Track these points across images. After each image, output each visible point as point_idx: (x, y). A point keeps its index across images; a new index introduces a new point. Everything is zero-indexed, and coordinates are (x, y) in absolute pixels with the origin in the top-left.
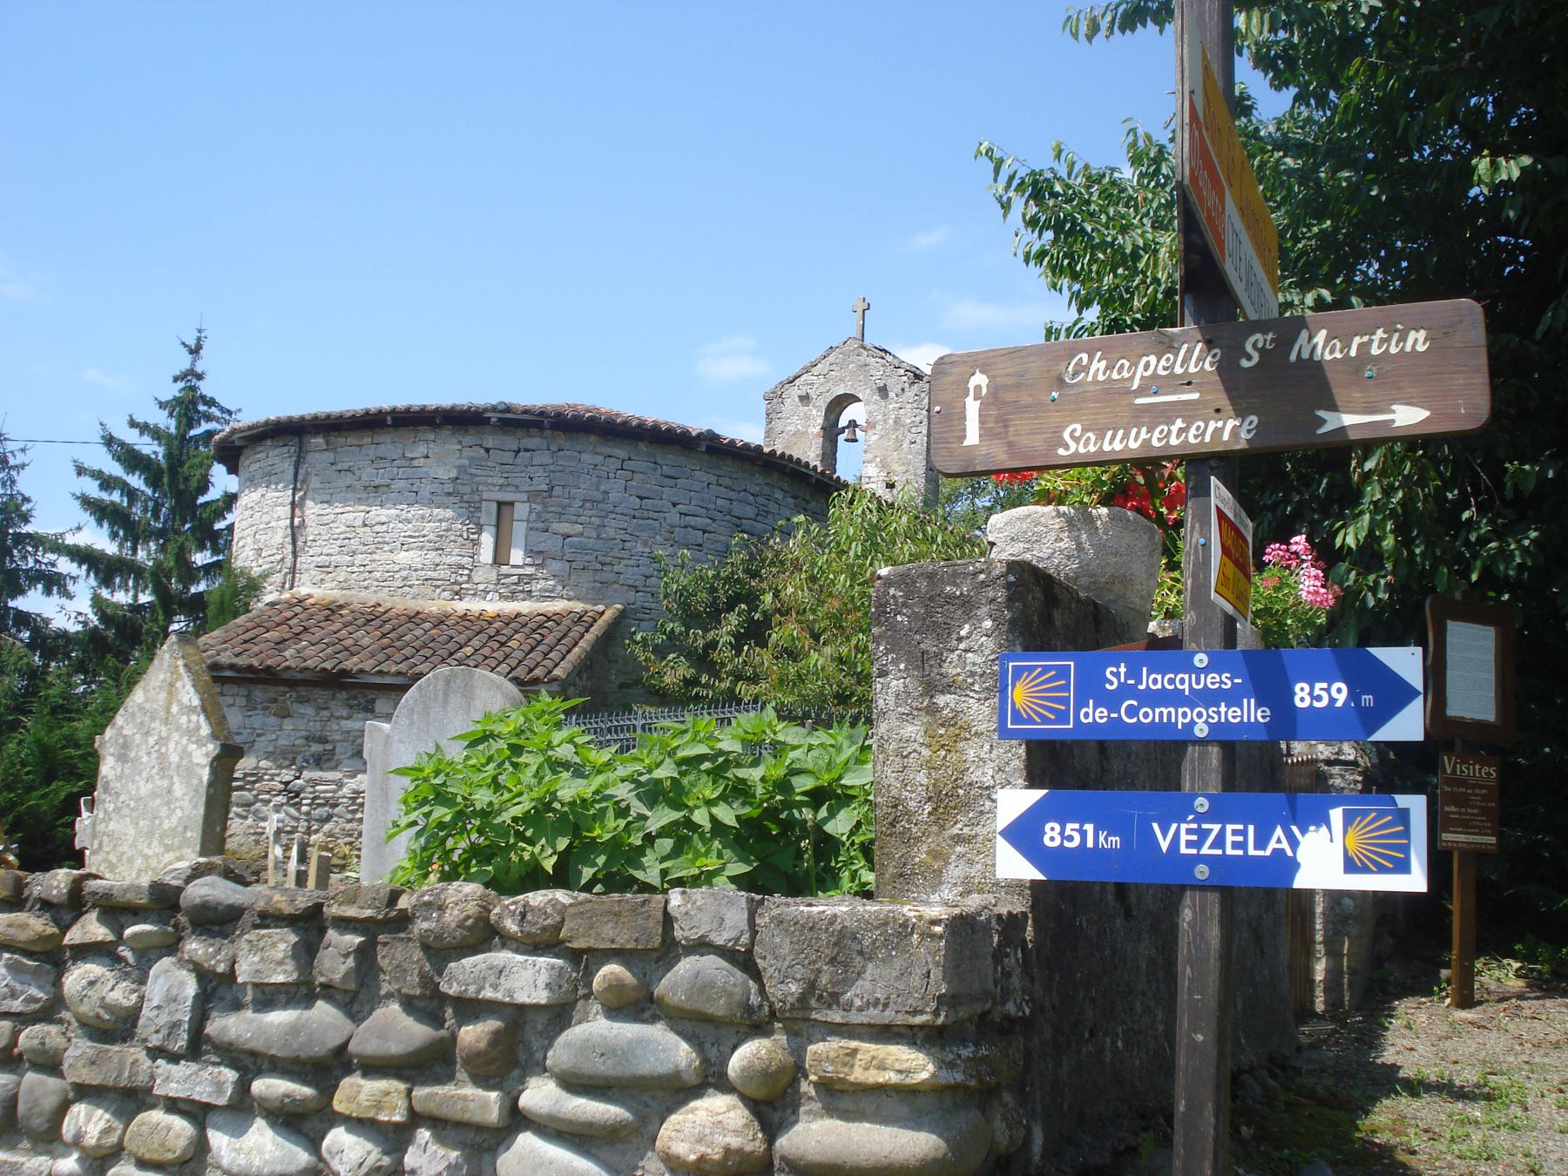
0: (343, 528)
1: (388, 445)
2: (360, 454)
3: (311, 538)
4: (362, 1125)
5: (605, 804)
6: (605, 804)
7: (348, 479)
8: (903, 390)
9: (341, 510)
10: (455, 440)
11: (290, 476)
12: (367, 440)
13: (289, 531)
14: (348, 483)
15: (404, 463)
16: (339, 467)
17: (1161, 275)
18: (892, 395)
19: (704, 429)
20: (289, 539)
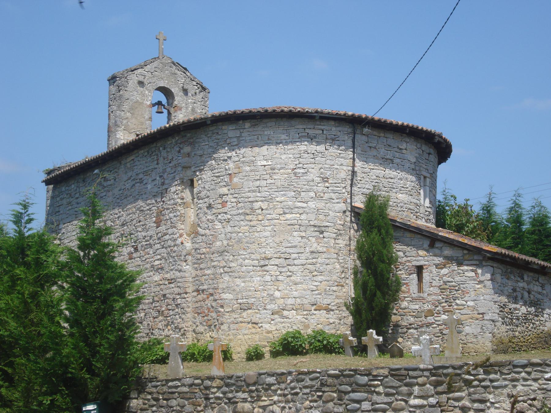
0: (375, 177)
1: (392, 139)
2: (300, 126)
3: (359, 178)
4: (547, 314)
5: (443, 378)
6: (443, 378)
7: (374, 152)
8: (196, 93)
9: (373, 167)
10: (415, 144)
11: (350, 143)
12: (382, 135)
13: (350, 173)
14: (375, 154)
15: (398, 150)
16: (370, 145)
17: (520, 388)
18: (190, 94)
19: (447, 161)
20: (350, 177)
